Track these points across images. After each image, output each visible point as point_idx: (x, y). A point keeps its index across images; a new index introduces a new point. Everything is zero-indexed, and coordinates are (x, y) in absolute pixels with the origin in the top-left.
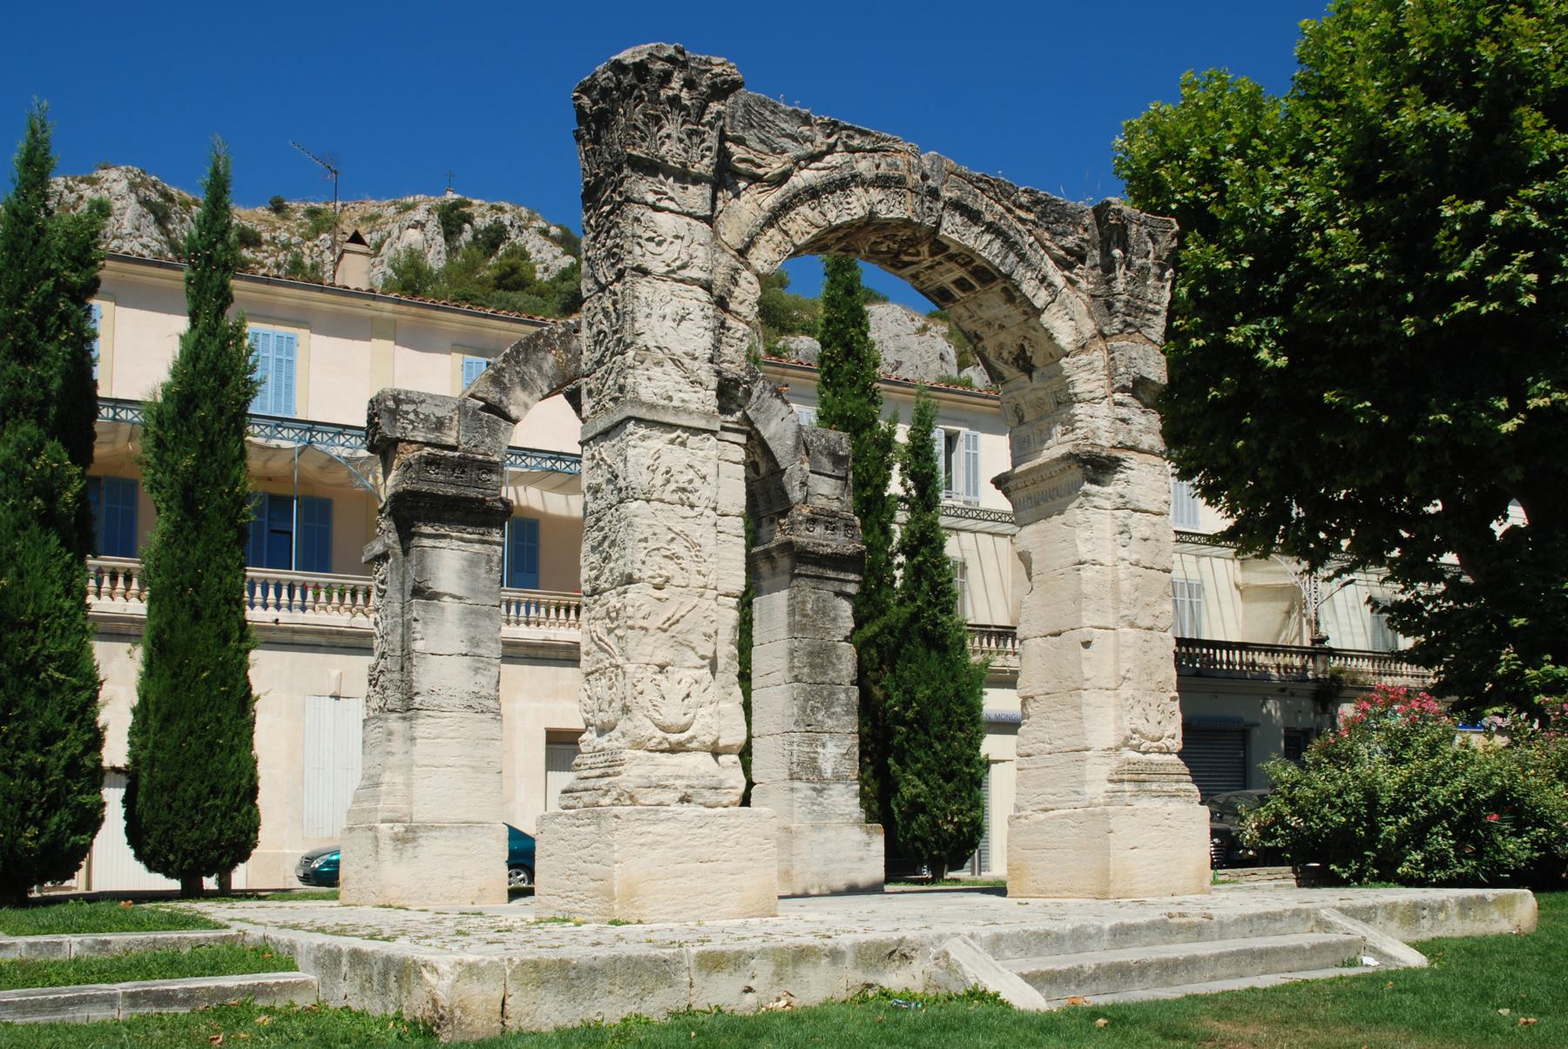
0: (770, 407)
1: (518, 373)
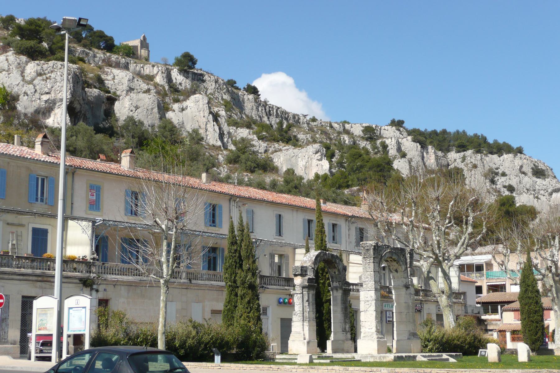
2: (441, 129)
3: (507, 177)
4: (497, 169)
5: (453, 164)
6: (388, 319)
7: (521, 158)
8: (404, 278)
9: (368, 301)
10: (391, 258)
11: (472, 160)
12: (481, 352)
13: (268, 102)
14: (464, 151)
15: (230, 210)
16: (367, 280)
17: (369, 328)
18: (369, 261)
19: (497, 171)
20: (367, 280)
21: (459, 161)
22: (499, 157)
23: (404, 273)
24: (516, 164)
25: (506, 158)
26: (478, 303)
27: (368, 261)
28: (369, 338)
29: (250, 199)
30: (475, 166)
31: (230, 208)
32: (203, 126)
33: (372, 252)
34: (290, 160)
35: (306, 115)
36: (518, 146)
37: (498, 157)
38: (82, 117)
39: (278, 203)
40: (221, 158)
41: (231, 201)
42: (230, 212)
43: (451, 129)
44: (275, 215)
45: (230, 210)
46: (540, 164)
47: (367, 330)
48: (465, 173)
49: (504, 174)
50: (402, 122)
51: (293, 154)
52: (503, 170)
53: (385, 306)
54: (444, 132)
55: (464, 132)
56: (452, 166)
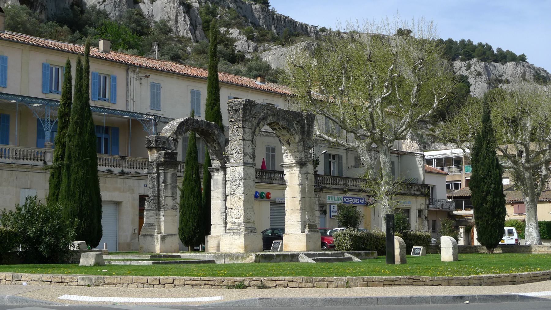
2: (447, 39)
3: (510, 84)
4: (501, 76)
5: (459, 72)
6: (332, 214)
7: (523, 66)
8: (298, 152)
9: (236, 180)
10: (278, 124)
11: (476, 68)
12: (415, 249)
13: (276, 11)
14: (469, 59)
15: (127, 82)
16: (234, 151)
17: (236, 216)
18: (238, 125)
19: (500, 78)
20: (234, 151)
21: (464, 69)
22: (503, 65)
23: (298, 146)
24: (519, 72)
25: (509, 65)
26: (449, 198)
27: (236, 126)
28: (235, 231)
29: (154, 70)
30: (479, 74)
31: (127, 79)
32: (173, 18)
33: (240, 113)
34: (278, 59)
35: (317, 27)
36: (521, 54)
37: (501, 65)
38: (38, 7)
39: (193, 77)
40: (189, 49)
41: (130, 72)
42: (127, 85)
43: (457, 38)
44: (190, 91)
45: (127, 82)
46: (541, 71)
47: (234, 220)
48: (471, 80)
49: (507, 81)
50: (409, 32)
51: (281, 53)
52: (506, 77)
53: (329, 199)
54: (450, 41)
55: (469, 41)
56: (458, 74)
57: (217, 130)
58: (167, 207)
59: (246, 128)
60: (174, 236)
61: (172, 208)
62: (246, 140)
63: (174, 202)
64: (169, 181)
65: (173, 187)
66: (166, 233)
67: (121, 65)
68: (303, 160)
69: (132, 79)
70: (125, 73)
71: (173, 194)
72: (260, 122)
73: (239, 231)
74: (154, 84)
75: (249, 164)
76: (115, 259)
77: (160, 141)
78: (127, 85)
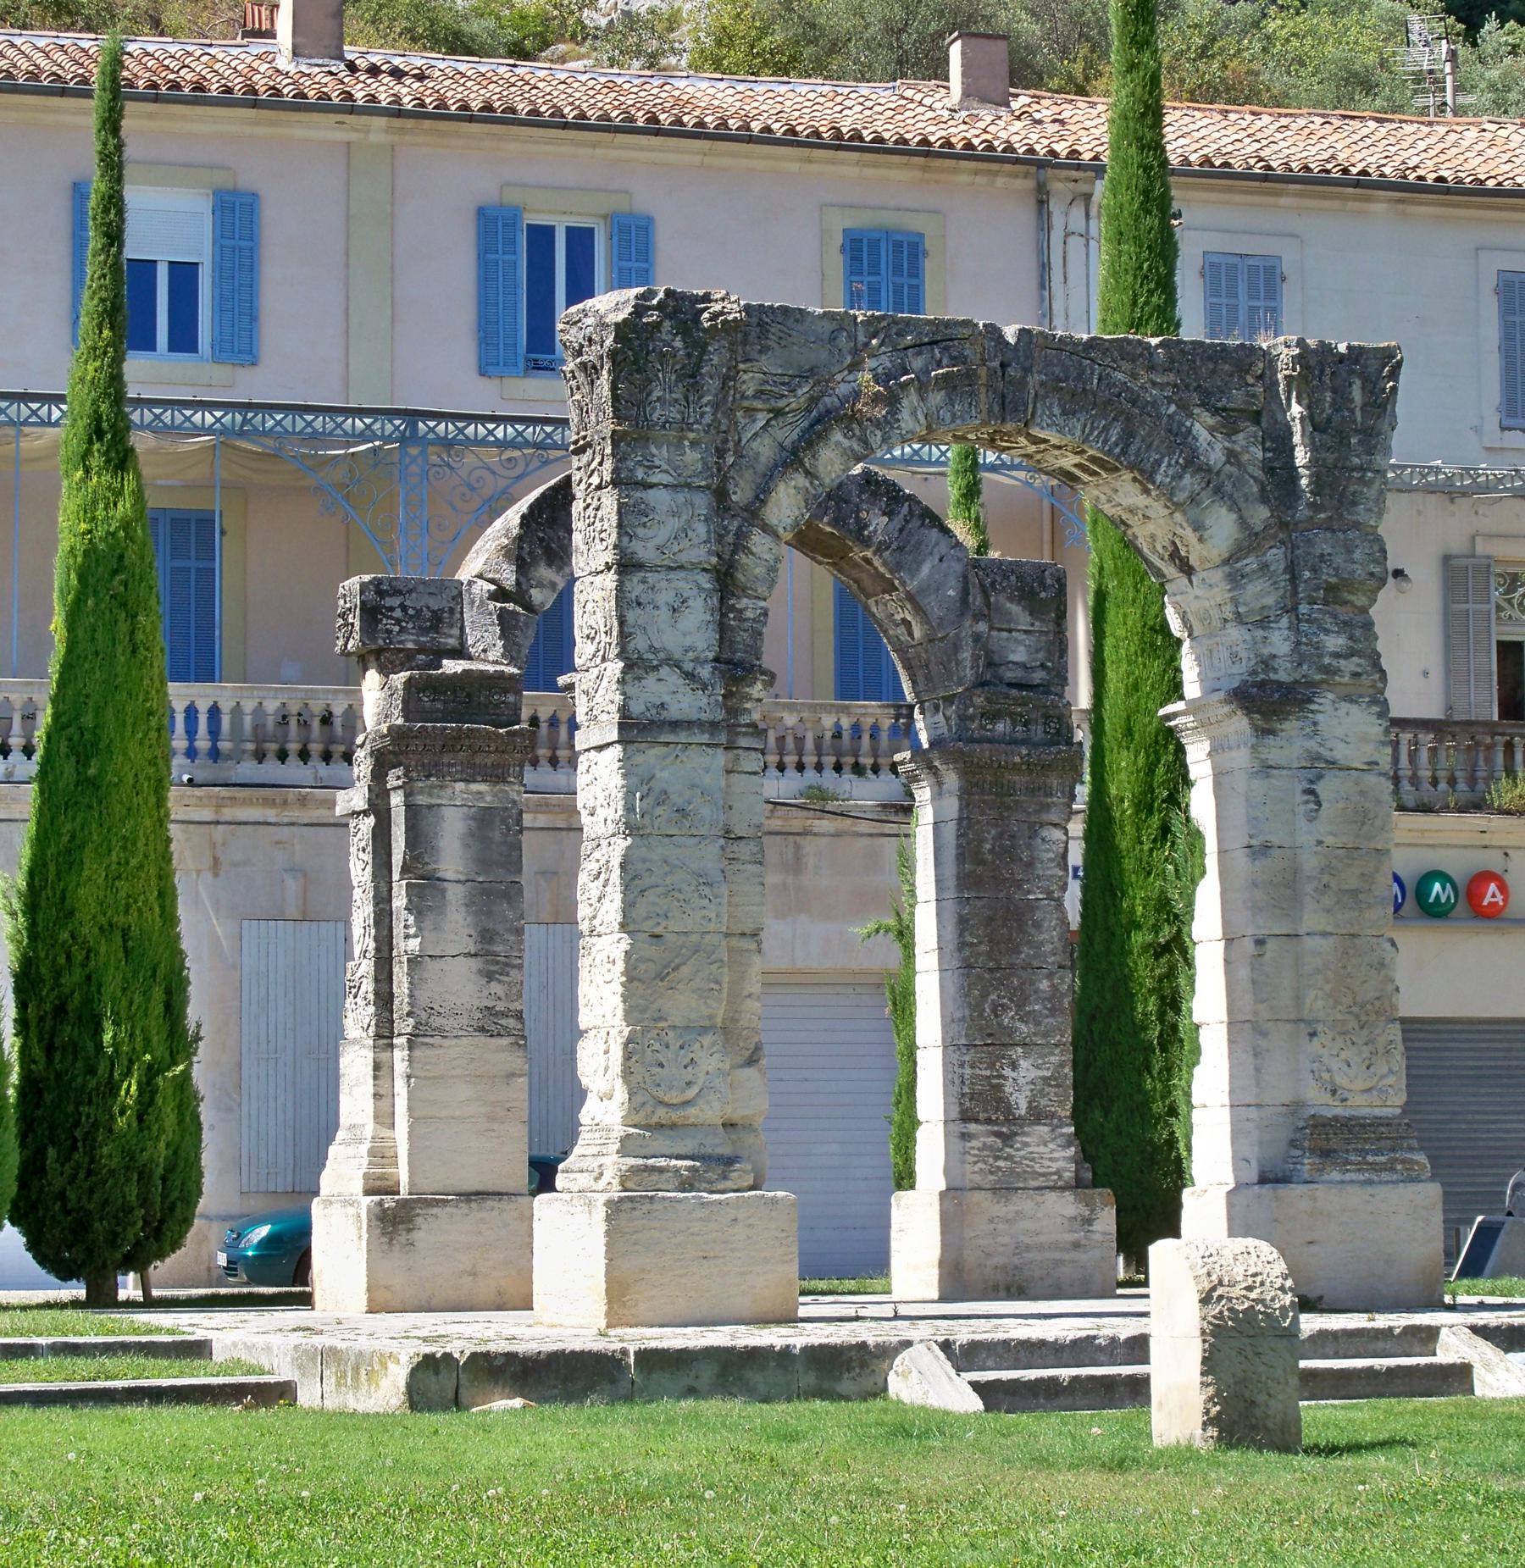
0: (920, 542)
1: (542, 540)
42: (1044, 283)
44: (1490, 282)
45: (1045, 268)
57: (889, 514)
58: (437, 1021)
59: (652, 486)
60: (490, 1203)
61: (482, 1029)
62: (655, 569)
63: (495, 988)
64: (452, 859)
65: (484, 892)
66: (425, 1185)
67: (996, 174)
68: (1282, 676)
69: (1075, 243)
70: (1025, 215)
71: (486, 936)
72: (822, 437)
73: (597, 1179)
74: (1236, 260)
75: (688, 725)
76: (95, 1346)
77: (404, 608)
78: (1044, 283)
